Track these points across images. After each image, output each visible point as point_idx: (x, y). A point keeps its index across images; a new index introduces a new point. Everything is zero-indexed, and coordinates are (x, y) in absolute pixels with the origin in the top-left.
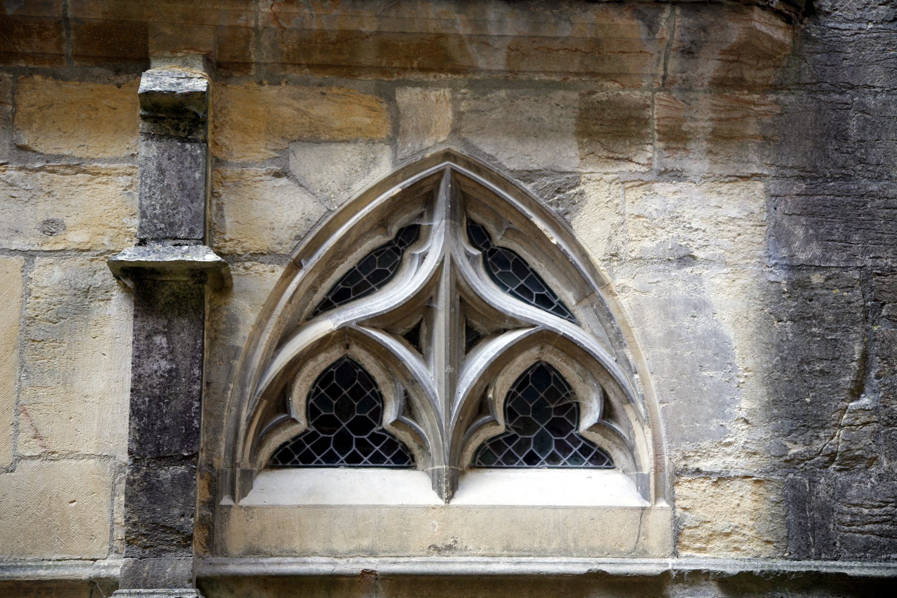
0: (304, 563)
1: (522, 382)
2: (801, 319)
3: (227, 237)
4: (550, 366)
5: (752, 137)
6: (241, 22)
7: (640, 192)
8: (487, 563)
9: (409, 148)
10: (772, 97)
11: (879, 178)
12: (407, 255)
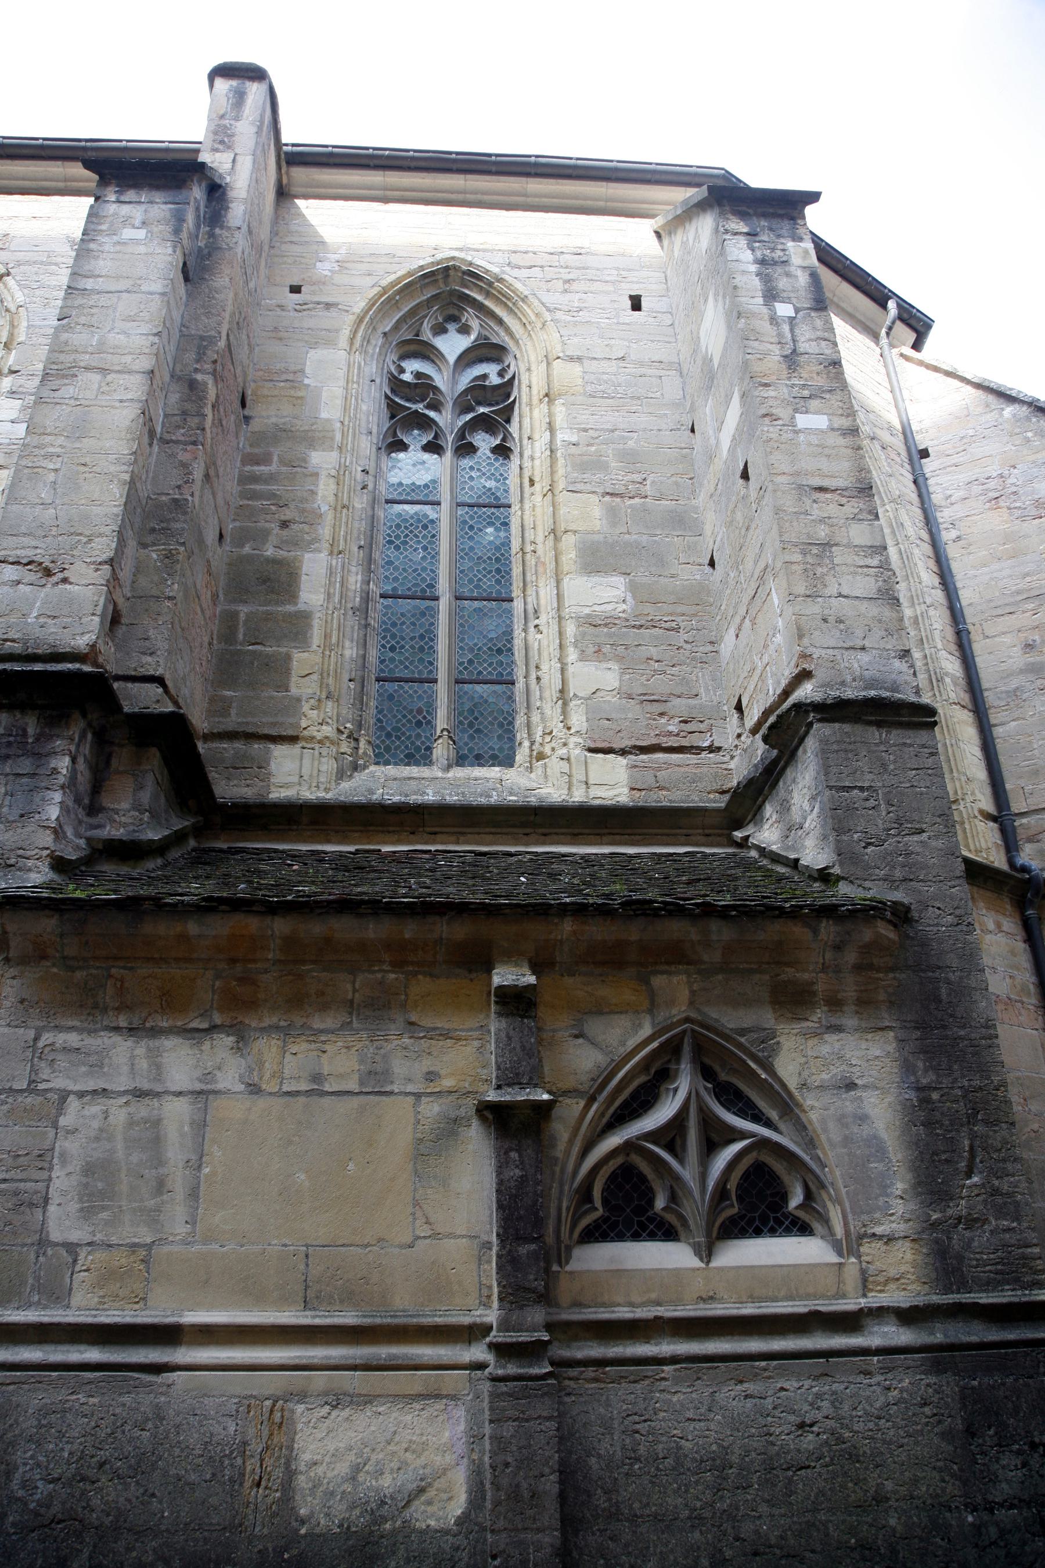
0: (613, 1312)
1: (746, 1176)
2: (929, 1124)
3: (546, 1080)
4: (764, 1164)
5: (883, 1001)
6: (552, 936)
7: (816, 1041)
8: (738, 1308)
9: (662, 1015)
10: (891, 975)
11: (964, 1027)
12: (662, 1088)
